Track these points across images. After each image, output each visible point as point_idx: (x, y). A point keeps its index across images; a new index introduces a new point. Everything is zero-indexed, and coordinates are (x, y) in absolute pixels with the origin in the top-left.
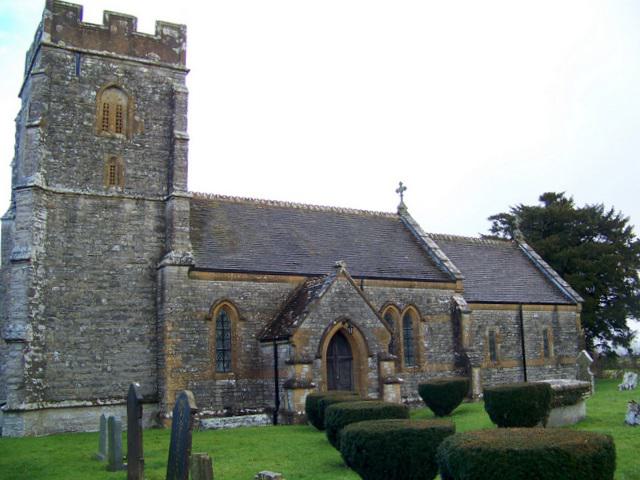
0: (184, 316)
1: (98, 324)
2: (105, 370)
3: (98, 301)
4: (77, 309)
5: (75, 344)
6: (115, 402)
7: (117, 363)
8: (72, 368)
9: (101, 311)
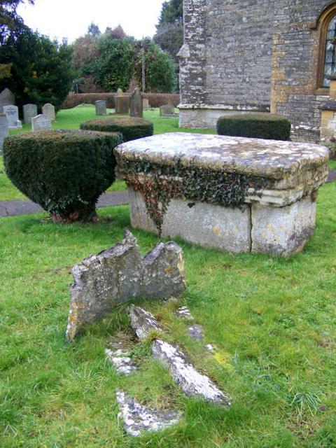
0: (290, 28)
1: (240, 41)
2: (244, 81)
3: (240, 20)
4: (225, 28)
5: (224, 59)
6: (249, 108)
7: (253, 75)
8: (222, 78)
9: (242, 29)
